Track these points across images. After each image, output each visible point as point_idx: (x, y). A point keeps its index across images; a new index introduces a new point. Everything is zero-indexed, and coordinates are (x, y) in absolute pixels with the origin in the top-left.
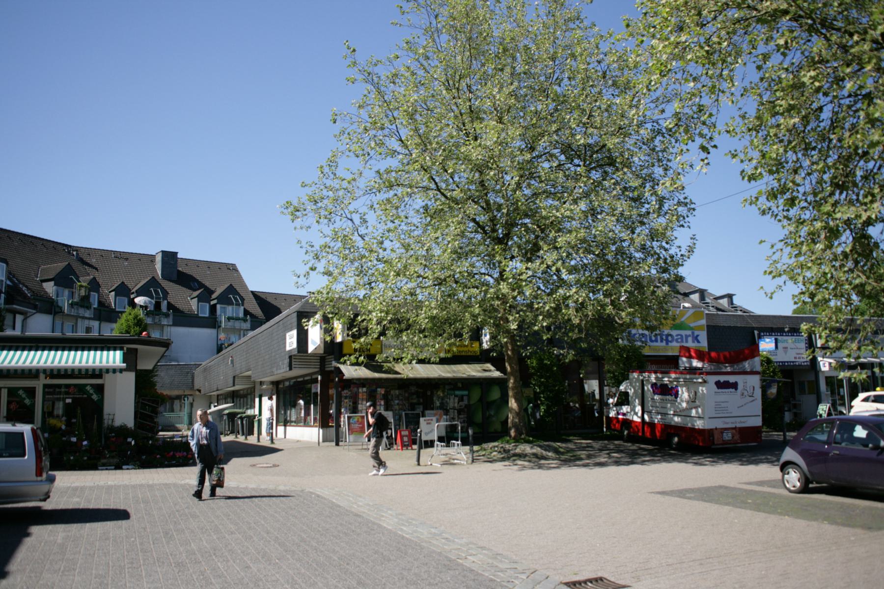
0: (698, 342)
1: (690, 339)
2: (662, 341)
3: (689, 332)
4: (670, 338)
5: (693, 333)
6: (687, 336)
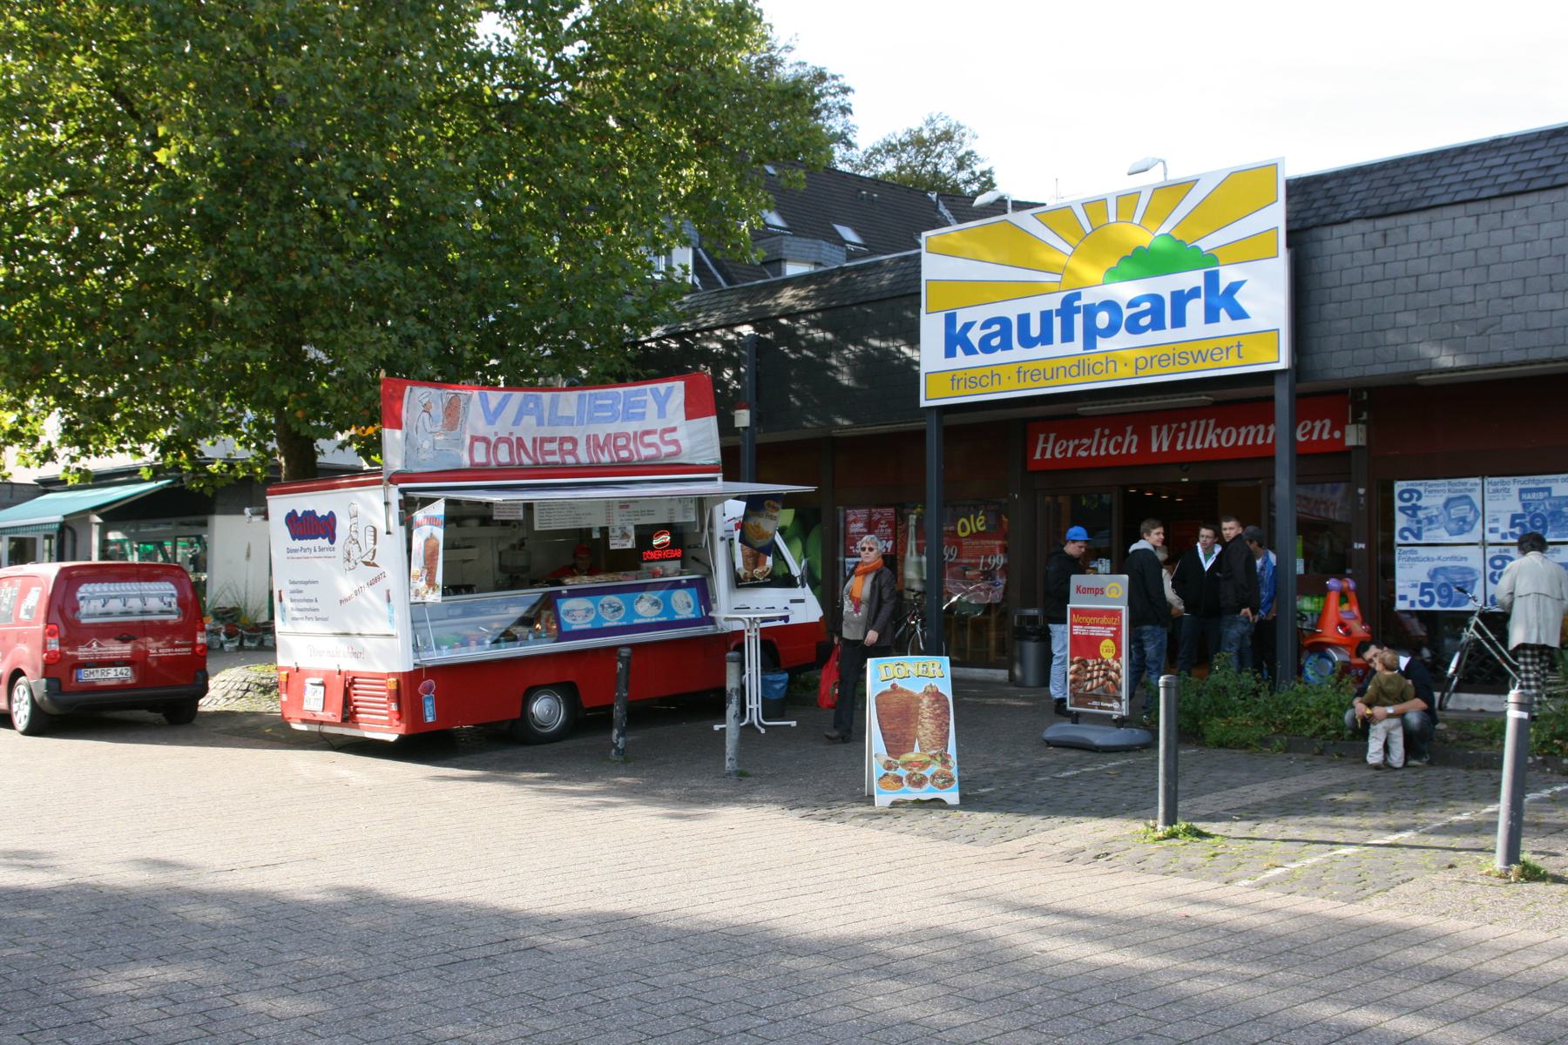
0: (1238, 314)
1: (1195, 309)
2: (1068, 336)
3: (1195, 279)
4: (1103, 319)
5: (1212, 279)
6: (1180, 299)
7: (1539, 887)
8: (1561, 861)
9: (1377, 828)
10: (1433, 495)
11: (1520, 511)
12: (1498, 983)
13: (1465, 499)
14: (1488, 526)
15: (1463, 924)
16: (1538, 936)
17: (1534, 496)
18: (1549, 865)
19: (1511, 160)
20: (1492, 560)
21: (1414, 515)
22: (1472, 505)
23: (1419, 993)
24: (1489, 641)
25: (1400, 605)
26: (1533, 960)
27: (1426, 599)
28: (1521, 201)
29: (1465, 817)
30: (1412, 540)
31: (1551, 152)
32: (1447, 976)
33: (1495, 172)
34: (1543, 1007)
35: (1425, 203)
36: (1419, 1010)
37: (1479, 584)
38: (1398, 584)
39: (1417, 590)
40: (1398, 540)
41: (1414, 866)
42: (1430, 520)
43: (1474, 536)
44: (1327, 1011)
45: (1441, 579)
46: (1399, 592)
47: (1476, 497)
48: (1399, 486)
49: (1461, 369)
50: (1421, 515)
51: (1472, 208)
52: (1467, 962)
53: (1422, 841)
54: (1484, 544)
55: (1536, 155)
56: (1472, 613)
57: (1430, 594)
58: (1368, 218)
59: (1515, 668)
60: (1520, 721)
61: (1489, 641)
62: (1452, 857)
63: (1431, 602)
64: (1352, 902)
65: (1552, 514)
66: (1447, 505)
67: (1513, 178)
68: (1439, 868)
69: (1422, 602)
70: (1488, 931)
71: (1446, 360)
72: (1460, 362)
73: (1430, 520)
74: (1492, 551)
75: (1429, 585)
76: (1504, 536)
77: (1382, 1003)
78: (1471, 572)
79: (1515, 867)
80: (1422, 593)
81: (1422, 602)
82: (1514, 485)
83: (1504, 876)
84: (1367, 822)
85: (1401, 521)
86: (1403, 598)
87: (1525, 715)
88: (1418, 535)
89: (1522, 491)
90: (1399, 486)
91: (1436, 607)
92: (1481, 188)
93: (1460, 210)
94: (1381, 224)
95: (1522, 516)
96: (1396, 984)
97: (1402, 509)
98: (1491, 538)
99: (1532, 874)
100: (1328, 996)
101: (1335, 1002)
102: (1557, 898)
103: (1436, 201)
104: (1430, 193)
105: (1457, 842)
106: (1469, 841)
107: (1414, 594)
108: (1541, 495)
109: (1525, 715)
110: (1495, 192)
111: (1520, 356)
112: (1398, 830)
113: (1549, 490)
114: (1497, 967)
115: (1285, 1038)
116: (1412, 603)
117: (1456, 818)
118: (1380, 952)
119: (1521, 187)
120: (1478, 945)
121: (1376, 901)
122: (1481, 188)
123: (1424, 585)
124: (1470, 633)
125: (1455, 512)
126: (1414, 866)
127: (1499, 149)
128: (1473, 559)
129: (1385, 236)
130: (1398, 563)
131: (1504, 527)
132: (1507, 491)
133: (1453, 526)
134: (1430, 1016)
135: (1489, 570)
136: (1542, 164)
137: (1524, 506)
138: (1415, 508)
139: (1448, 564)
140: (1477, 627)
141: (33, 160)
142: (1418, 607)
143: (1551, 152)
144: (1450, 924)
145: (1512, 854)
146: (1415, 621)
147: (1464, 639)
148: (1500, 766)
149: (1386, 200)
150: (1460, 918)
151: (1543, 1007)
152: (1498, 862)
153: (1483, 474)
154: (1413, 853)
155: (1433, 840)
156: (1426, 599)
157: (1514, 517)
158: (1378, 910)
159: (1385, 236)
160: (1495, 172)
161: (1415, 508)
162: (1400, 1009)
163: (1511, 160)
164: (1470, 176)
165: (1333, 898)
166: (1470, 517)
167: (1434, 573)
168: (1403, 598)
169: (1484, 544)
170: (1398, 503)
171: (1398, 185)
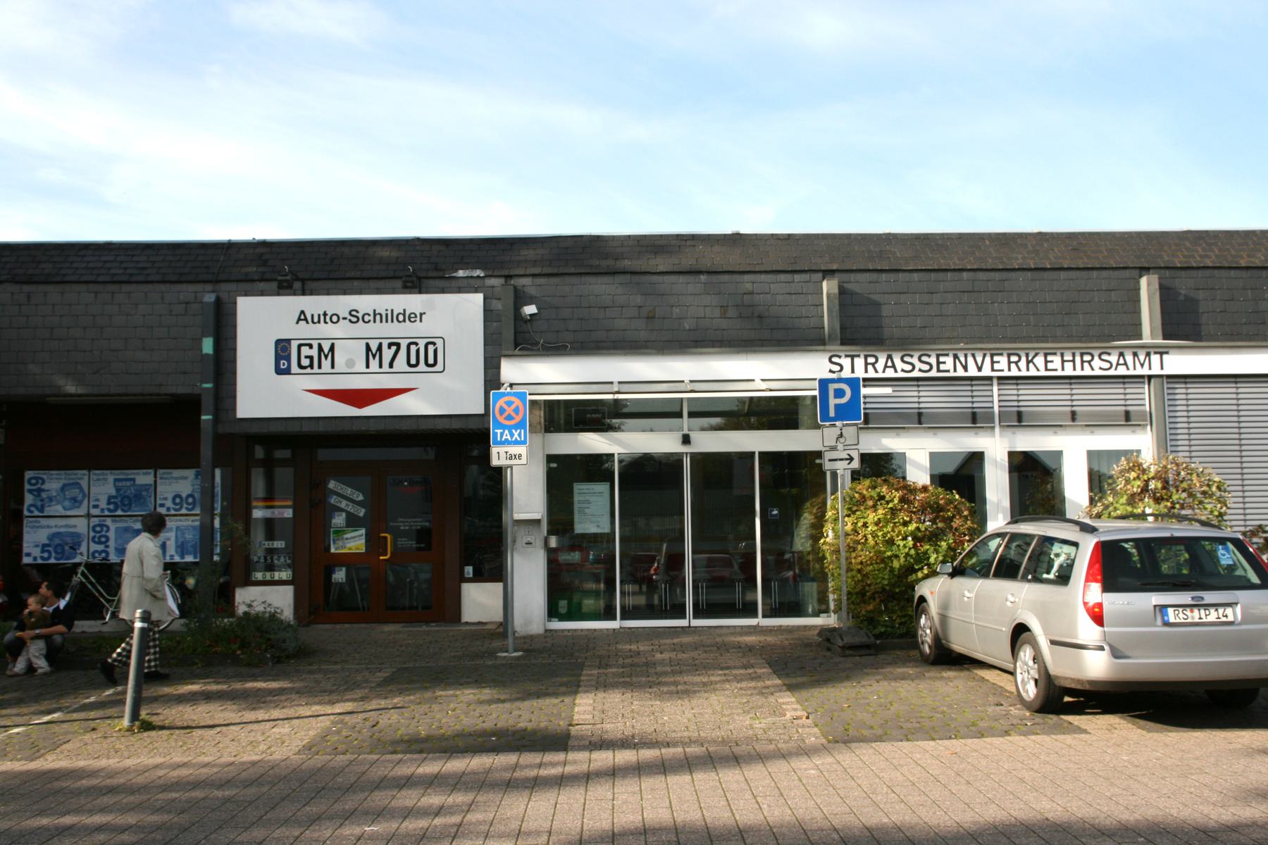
7: (153, 733)
8: (161, 717)
9: (34, 713)
10: (53, 482)
11: (114, 493)
12: (145, 788)
13: (77, 485)
14: (92, 503)
15: (111, 761)
16: (159, 760)
17: (124, 483)
18: (155, 720)
19: (119, 259)
20: (94, 527)
21: (39, 495)
22: (81, 489)
23: (98, 801)
24: (91, 583)
25: (26, 560)
26: (161, 773)
27: (46, 555)
28: (125, 288)
29: (92, 699)
30: (36, 513)
31: (145, 258)
32: (112, 790)
33: (108, 265)
34: (175, 795)
35: (59, 279)
36: (102, 810)
37: (84, 544)
38: (25, 545)
39: (39, 549)
40: (26, 513)
41: (67, 733)
42: (51, 499)
43: (82, 511)
44: (45, 821)
45: (57, 541)
46: (25, 550)
47: (84, 484)
48: (29, 474)
49: (87, 395)
50: (44, 495)
51: (93, 287)
52: (122, 781)
53: (69, 717)
54: (89, 516)
55: (135, 259)
56: (79, 564)
57: (49, 552)
58: (17, 282)
59: (108, 601)
60: (142, 629)
61: (91, 583)
62: (92, 724)
63: (49, 558)
64: (32, 760)
65: (136, 496)
66: (63, 488)
67: (121, 271)
68: (86, 732)
69: (42, 558)
70: (129, 763)
71: (71, 389)
72: (80, 391)
73: (51, 499)
74: (95, 521)
75: (48, 545)
76: (102, 510)
77: (78, 811)
78: (78, 535)
79: (137, 723)
80: (43, 551)
81: (42, 558)
82: (111, 476)
83: (130, 729)
84: (25, 710)
85: (29, 499)
86: (28, 555)
87: (146, 625)
88: (42, 510)
89: (116, 480)
90: (29, 474)
91: (52, 561)
92: (98, 275)
93: (83, 287)
94: (26, 288)
95: (115, 497)
96: (83, 800)
97: (30, 491)
98: (94, 512)
99: (148, 726)
100: (41, 813)
101: (47, 816)
102: (165, 738)
103: (67, 279)
104: (63, 272)
105: (92, 714)
106: (99, 713)
107: (36, 552)
108: (128, 483)
109: (146, 625)
110: (108, 278)
111: (121, 390)
112: (49, 712)
113: (134, 480)
114: (141, 780)
115: (23, 840)
116: (35, 559)
117: (87, 701)
118: (64, 785)
119: (125, 278)
120: (126, 770)
121: (50, 757)
122: (98, 275)
123: (44, 546)
124: (78, 578)
125: (68, 494)
126: (67, 733)
127: (110, 250)
128: (81, 526)
129: (29, 297)
130: (25, 530)
131: (103, 504)
132: (105, 480)
133: (67, 503)
134: (111, 812)
135: (92, 534)
136: (140, 265)
137: (118, 490)
138: (40, 491)
139: (62, 530)
140: (83, 574)
141: (636, 581)
142: (40, 561)
143: (145, 258)
144: (103, 763)
145: (135, 716)
146: (34, 572)
147: (73, 583)
148: (681, 513)
149: (30, 272)
150: (108, 758)
151: (175, 795)
152: (126, 722)
153: (90, 468)
154: (65, 726)
155: (75, 716)
156: (46, 555)
157: (110, 498)
158: (51, 762)
159: (29, 297)
160: (108, 265)
161: (40, 491)
162: (91, 812)
163: (119, 259)
164: (90, 265)
165: (19, 760)
166: (80, 497)
167: (52, 537)
168: (28, 555)
169: (89, 516)
170: (27, 487)
171: (40, 262)
